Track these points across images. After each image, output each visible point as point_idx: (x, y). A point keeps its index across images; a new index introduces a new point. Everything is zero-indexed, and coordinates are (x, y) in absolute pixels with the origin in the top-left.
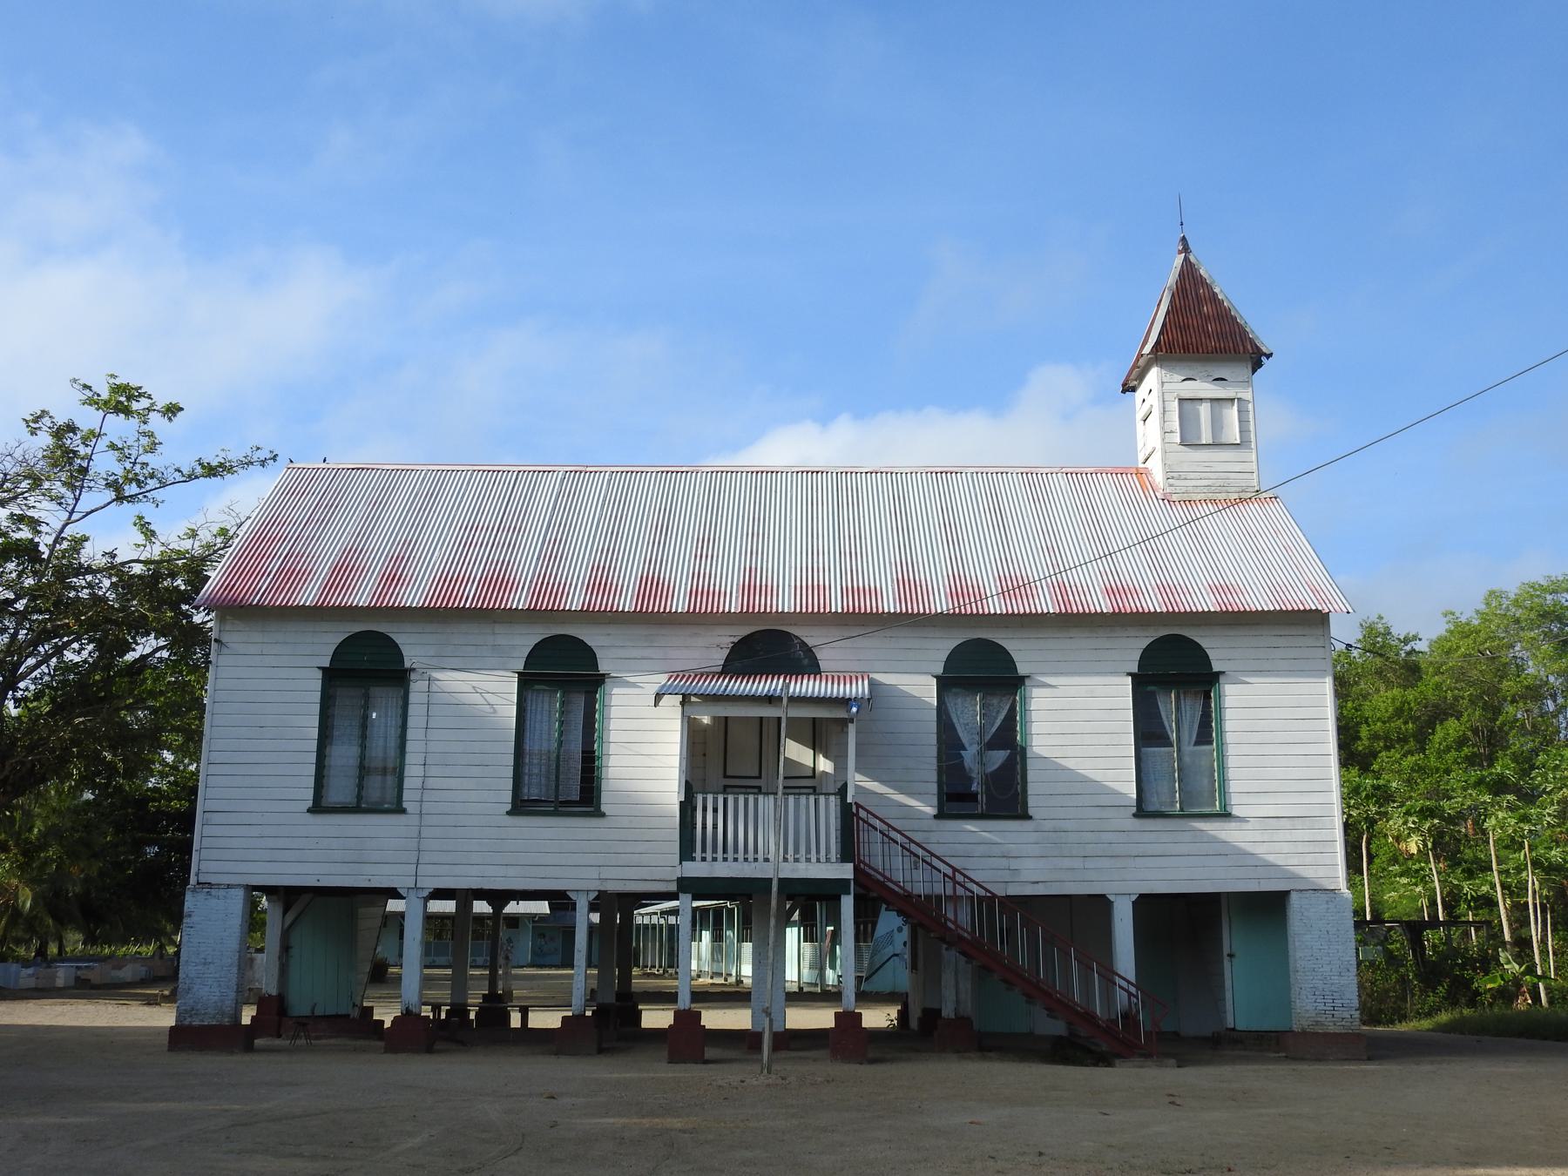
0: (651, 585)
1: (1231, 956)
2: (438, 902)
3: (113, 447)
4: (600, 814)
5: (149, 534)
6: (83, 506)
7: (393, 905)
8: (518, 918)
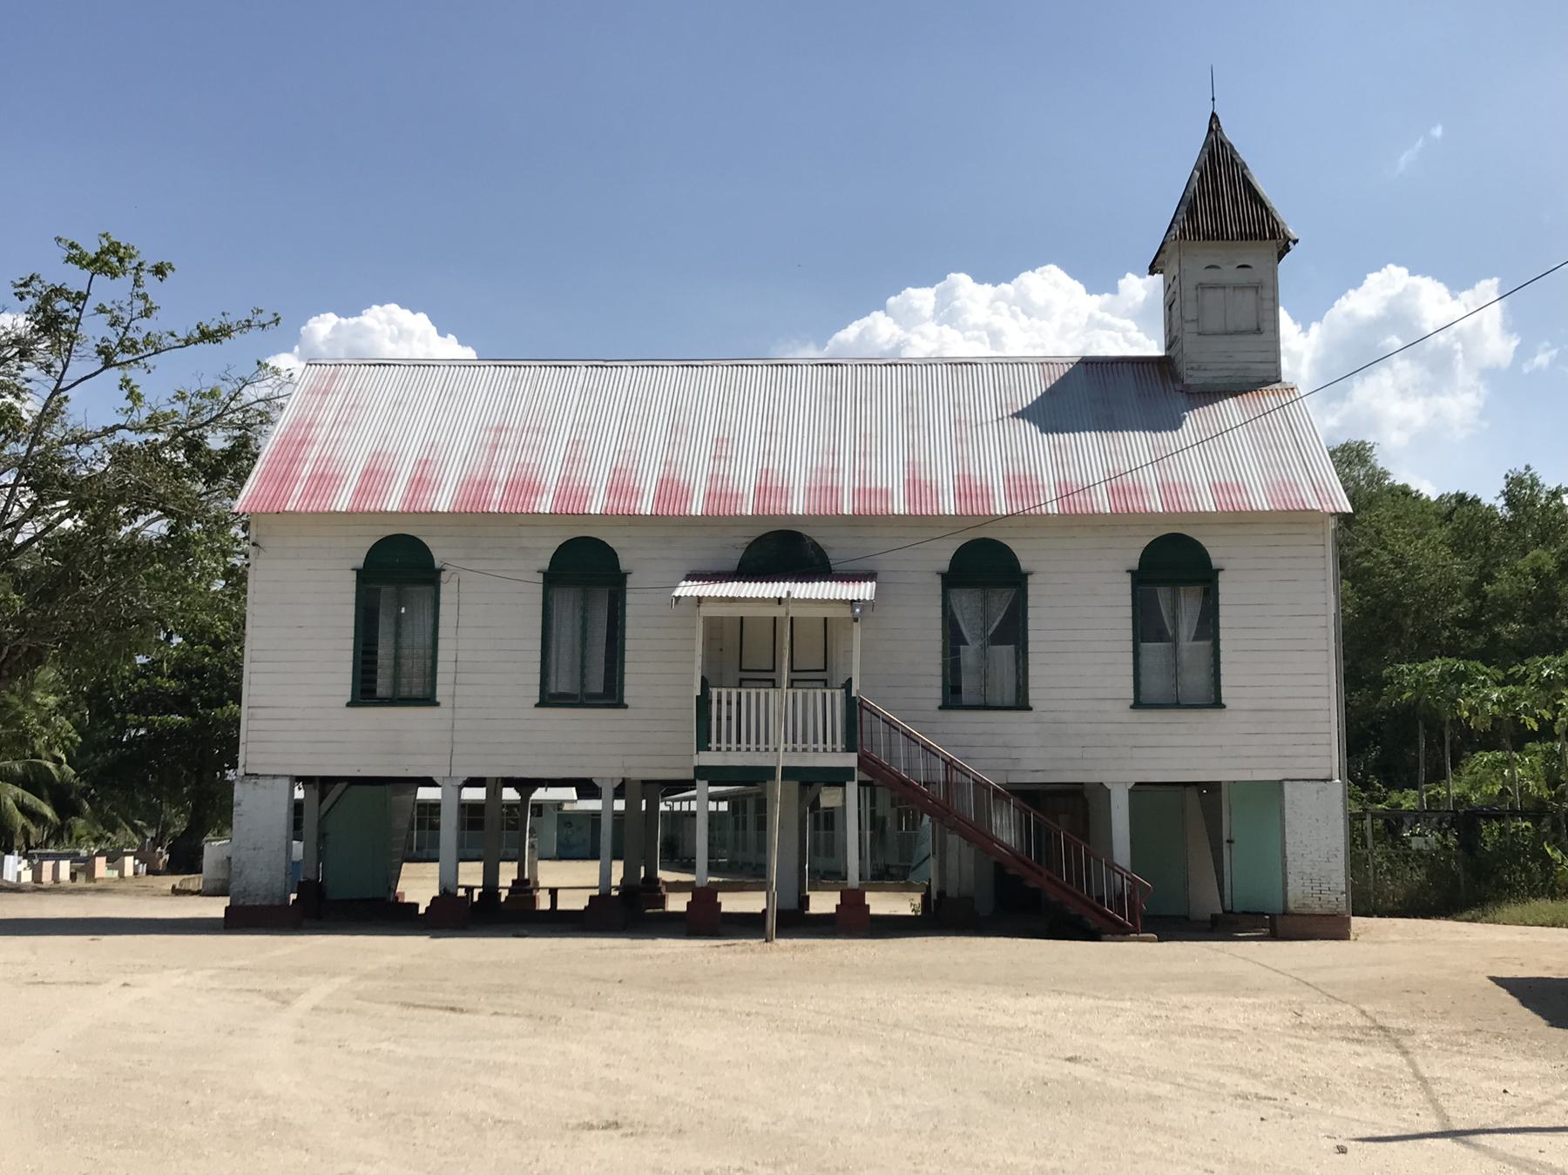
0: (670, 488)
1: (1230, 841)
2: (44, 874)
3: (101, 310)
4: (621, 705)
5: (134, 396)
6: (72, 374)
7: (424, 793)
8: (541, 805)
